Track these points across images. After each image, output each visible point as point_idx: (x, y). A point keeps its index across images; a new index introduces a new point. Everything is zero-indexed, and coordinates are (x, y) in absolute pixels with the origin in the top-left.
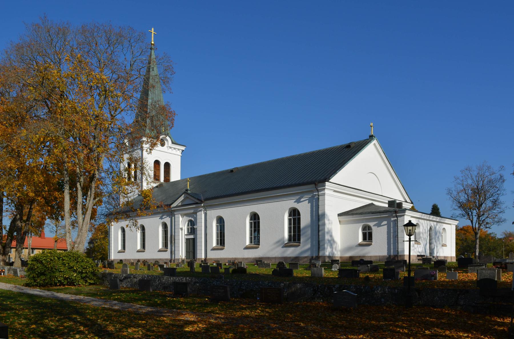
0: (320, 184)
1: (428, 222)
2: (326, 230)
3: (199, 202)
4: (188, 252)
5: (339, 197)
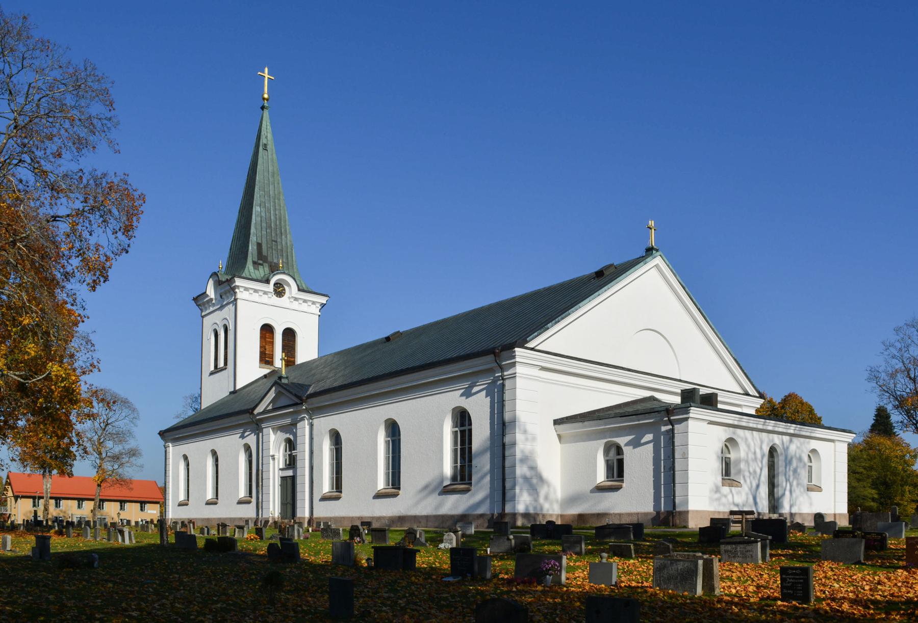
0: (504, 354)
1: (764, 434)
2: (519, 455)
3: (299, 401)
4: (284, 504)
5: (567, 385)
